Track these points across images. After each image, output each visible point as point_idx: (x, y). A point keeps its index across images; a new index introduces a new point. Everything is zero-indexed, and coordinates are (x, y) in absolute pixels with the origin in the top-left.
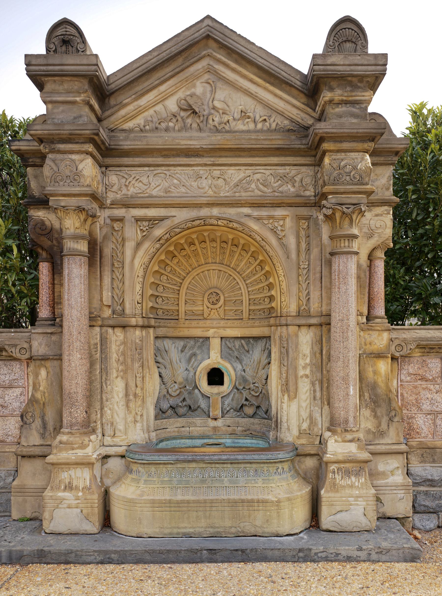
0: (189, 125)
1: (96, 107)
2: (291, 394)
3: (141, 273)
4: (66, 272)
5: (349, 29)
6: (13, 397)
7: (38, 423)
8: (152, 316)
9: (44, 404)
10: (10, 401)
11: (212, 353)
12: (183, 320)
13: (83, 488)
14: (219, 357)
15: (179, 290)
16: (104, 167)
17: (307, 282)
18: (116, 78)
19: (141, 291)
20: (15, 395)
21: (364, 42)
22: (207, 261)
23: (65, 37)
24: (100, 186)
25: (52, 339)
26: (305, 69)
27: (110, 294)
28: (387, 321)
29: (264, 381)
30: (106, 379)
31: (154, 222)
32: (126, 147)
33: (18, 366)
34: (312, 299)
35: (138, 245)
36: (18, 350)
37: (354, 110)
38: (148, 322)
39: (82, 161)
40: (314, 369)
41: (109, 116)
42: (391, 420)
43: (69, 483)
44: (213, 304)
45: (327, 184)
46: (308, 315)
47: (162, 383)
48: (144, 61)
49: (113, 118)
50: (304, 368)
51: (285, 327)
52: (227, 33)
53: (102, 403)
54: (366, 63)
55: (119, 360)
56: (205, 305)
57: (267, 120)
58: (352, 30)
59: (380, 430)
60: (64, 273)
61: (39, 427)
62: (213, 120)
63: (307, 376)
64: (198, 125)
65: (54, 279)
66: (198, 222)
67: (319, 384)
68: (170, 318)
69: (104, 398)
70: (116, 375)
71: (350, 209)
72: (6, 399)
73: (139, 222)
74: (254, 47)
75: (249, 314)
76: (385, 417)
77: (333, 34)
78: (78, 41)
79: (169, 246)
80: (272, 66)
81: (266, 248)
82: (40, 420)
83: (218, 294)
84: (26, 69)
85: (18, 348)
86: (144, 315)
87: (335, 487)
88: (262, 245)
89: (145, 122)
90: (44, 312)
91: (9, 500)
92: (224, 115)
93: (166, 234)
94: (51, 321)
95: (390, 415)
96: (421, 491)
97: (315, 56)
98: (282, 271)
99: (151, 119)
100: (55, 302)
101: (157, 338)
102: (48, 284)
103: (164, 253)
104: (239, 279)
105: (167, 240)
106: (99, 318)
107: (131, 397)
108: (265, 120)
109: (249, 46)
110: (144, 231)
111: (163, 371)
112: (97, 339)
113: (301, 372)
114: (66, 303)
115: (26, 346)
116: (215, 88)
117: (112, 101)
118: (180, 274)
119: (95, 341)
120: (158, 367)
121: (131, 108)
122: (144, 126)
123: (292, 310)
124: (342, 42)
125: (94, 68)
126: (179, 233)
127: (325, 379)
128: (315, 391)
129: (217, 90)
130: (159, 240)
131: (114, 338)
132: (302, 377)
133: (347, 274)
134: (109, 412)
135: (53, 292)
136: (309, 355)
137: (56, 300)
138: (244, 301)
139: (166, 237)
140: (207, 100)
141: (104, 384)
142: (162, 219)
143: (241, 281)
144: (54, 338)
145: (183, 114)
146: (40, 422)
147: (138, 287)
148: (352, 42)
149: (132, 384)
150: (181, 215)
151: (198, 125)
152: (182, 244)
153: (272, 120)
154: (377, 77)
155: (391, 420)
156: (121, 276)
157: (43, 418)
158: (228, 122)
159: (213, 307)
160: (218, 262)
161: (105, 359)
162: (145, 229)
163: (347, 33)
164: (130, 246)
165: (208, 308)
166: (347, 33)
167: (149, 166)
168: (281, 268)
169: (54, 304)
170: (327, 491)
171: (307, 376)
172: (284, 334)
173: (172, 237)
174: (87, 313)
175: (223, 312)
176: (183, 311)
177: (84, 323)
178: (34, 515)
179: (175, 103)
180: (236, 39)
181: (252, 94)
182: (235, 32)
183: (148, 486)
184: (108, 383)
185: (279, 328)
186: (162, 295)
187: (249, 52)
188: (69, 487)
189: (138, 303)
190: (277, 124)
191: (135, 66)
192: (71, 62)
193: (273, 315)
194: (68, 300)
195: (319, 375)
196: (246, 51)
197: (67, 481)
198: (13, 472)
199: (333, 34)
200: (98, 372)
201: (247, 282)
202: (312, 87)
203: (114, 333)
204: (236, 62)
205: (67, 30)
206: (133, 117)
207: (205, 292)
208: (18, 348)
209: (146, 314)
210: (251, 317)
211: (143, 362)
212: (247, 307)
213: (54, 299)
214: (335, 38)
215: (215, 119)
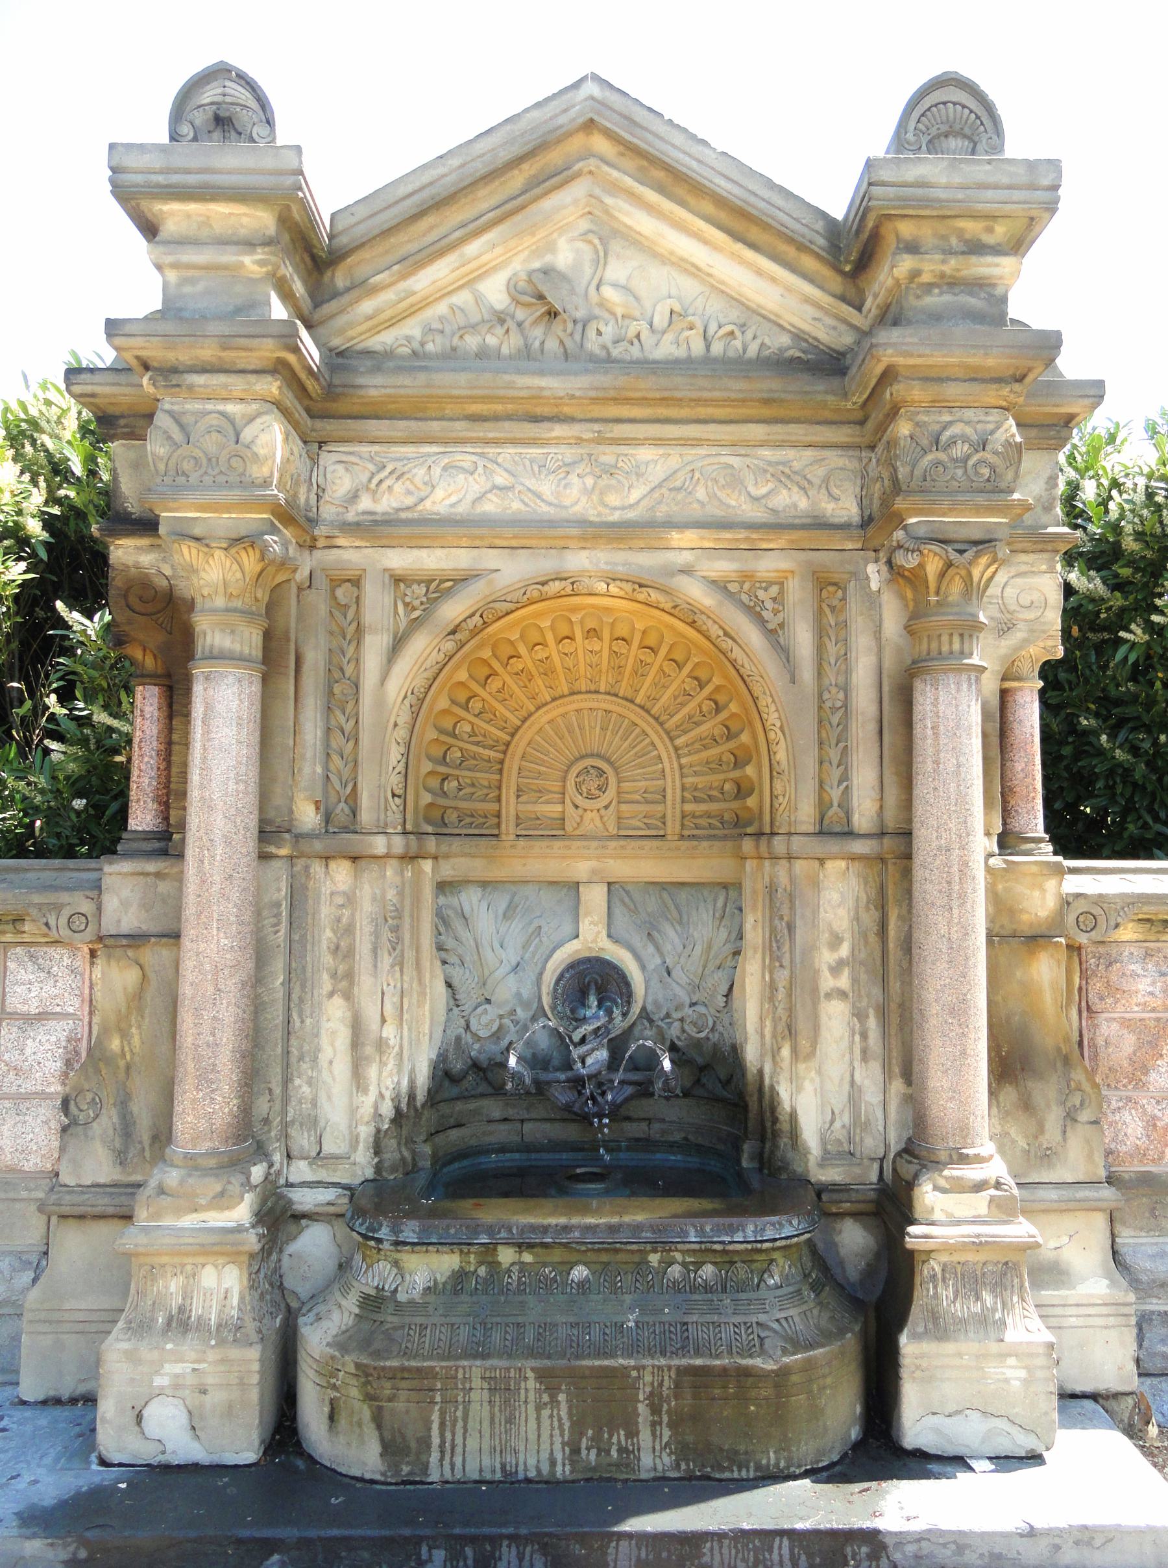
0: (537, 344)
1: (299, 288)
2: (804, 1043)
3: (404, 718)
4: (198, 710)
5: (955, 104)
6: (47, 1046)
7: (108, 1120)
8: (430, 829)
9: (128, 1068)
10: (39, 1056)
11: (585, 926)
12: (513, 837)
13: (219, 1326)
14: (604, 933)
15: (502, 762)
16: (315, 444)
17: (841, 745)
18: (353, 220)
19: (402, 764)
20: (53, 1039)
21: (995, 137)
23: (220, 109)
24: (303, 490)
25: (160, 889)
26: (838, 210)
27: (319, 770)
28: (1050, 848)
29: (721, 1001)
30: (301, 1000)
31: (440, 587)
32: (373, 392)
33: (67, 961)
34: (855, 788)
35: (397, 645)
36: (63, 921)
37: (972, 301)
38: (420, 847)
39: (251, 419)
40: (863, 977)
41: (333, 316)
42: (1070, 1117)
43: (181, 1310)
45: (904, 487)
46: (846, 829)
47: (452, 1002)
48: (426, 178)
49: (341, 320)
50: (835, 970)
51: (784, 862)
52: (640, 115)
53: (287, 1066)
54: (1005, 180)
55: (337, 948)
56: (568, 801)
57: (738, 333)
58: (964, 107)
59: (1040, 1145)
60: (194, 715)
61: (111, 1132)
62: (599, 333)
63: (843, 994)
64: (562, 342)
66: (555, 587)
67: (877, 1017)
68: (477, 832)
69: (295, 1052)
70: (330, 988)
71: (966, 555)
72: (28, 1051)
73: (402, 585)
74: (707, 151)
75: (683, 825)
76: (1054, 1108)
77: (916, 115)
78: (255, 119)
79: (480, 647)
80: (752, 199)
81: (733, 656)
82: (114, 1112)
83: (601, 772)
84: (111, 180)
85: (66, 913)
86: (409, 827)
87: (939, 1328)
88: (724, 646)
89: (424, 334)
90: (142, 817)
91: (16, 1339)
92: (627, 321)
93: (473, 615)
94: (159, 839)
95: (1069, 1104)
96: (1152, 1312)
97: (870, 164)
98: (776, 715)
99: (440, 327)
100: (172, 793)
101: (442, 887)
102: (155, 744)
103: (465, 666)
104: (657, 732)
105: (475, 632)
106: (287, 836)
107: (369, 1050)
108: (732, 333)
109: (697, 149)
110: (414, 609)
111: (457, 975)
112: (279, 890)
113: (828, 982)
114: (194, 794)
115: (86, 907)
116: (606, 254)
117: (340, 278)
118: (685, 732)
119: (275, 897)
120: (444, 962)
121: (388, 296)
122: (422, 344)
123: (804, 818)
124: (938, 136)
125: (289, 181)
126: (508, 614)
127: (893, 1006)
128: (864, 1036)
129: (610, 259)
130: (453, 632)
131: (326, 889)
132: (828, 996)
133: (958, 727)
134: (306, 1089)
135: (168, 768)
136: (847, 935)
137: (172, 786)
138: (669, 791)
139: (470, 624)
140: (584, 282)
141: (295, 1016)
142: (462, 580)
143: (661, 739)
144: (163, 887)
145: (520, 314)
146: (115, 1119)
147: (395, 754)
148: (965, 136)
149: (371, 1012)
150: (510, 570)
151: (562, 342)
152: (512, 643)
153: (749, 335)
154: (1032, 219)
155: (1070, 1117)
156: (352, 722)
157: (123, 1104)
158: (638, 336)
159: (587, 804)
160: (602, 690)
161: (297, 947)
162: (416, 603)
163: (950, 114)
164: (374, 648)
165: (577, 807)
166: (950, 114)
167: (390, 206)
168: (773, 708)
169: (168, 795)
170: (915, 1336)
171: (843, 994)
172: (783, 879)
173: (486, 624)
174: (253, 822)
175: (613, 818)
176: (512, 812)
177: (244, 850)
178: (82, 1389)
179: (504, 288)
180: (662, 129)
181: (699, 269)
182: (660, 115)
183: (407, 1320)
184: (307, 1009)
185: (767, 863)
186: (457, 772)
187: (694, 164)
188: (180, 1321)
189: (394, 795)
190: (762, 344)
191: (402, 191)
192: (229, 160)
193: (749, 830)
194: (202, 787)
195: (877, 991)
196: (687, 160)
197: (175, 1302)
198: (34, 1259)
199: (916, 115)
200: (281, 980)
201: (678, 742)
202: (852, 249)
203: (327, 873)
204: (661, 190)
205: (227, 90)
206: (392, 322)
207: (569, 767)
208: (66, 913)
209: (416, 824)
210: (686, 833)
211: (402, 951)
212: (678, 806)
213: (169, 782)
214: (920, 126)
215: (603, 329)
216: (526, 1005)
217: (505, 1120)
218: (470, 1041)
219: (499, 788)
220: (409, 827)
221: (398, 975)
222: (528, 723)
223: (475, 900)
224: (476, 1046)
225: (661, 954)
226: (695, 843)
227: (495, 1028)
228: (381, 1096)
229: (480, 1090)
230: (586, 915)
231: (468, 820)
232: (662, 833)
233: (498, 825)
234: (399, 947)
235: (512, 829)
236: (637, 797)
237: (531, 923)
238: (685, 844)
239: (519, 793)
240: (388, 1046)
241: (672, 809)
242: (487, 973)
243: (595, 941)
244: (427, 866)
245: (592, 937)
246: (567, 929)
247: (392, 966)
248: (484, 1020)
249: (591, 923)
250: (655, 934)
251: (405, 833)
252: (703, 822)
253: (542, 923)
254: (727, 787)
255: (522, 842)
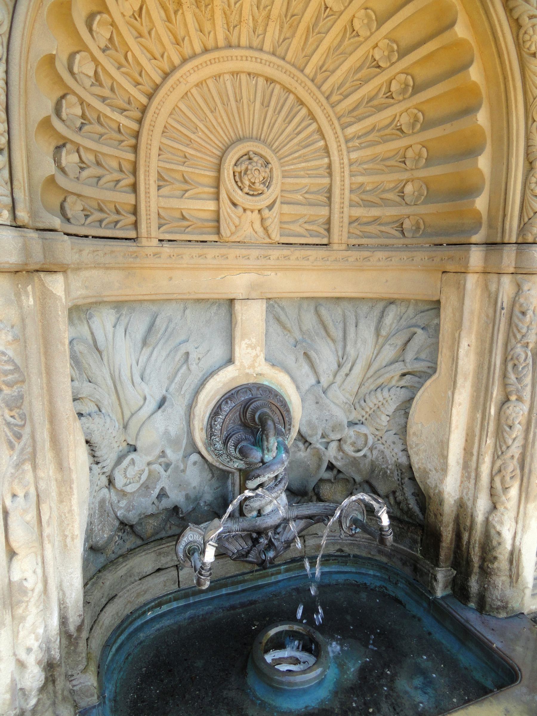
11: (242, 350)
12: (155, 242)
22: (187, 51)
38: (47, 250)
44: (254, 193)
56: (223, 195)
65: (30, 409)
165: (235, 205)
209: (33, 214)
216: (174, 443)
217: (159, 570)
218: (114, 498)
219: (134, 172)
220: (23, 215)
221: (29, 476)
222: (171, 81)
223: (109, 327)
224: (123, 503)
225: (316, 373)
226: (366, 254)
227: (144, 477)
228: (21, 665)
229: (128, 545)
230: (242, 338)
231: (97, 215)
232: (325, 241)
233: (136, 225)
234: (26, 431)
235: (154, 233)
236: (299, 197)
237: (176, 349)
238: (354, 254)
239: (162, 181)
240: (24, 591)
241: (342, 211)
242: (127, 414)
243: (252, 366)
244: (57, 284)
245: (252, 362)
246: (218, 352)
247: (18, 466)
248: (132, 472)
249: (249, 346)
250: (312, 354)
251: (17, 225)
252: (372, 229)
253: (189, 347)
254: (409, 189)
255: (167, 249)
